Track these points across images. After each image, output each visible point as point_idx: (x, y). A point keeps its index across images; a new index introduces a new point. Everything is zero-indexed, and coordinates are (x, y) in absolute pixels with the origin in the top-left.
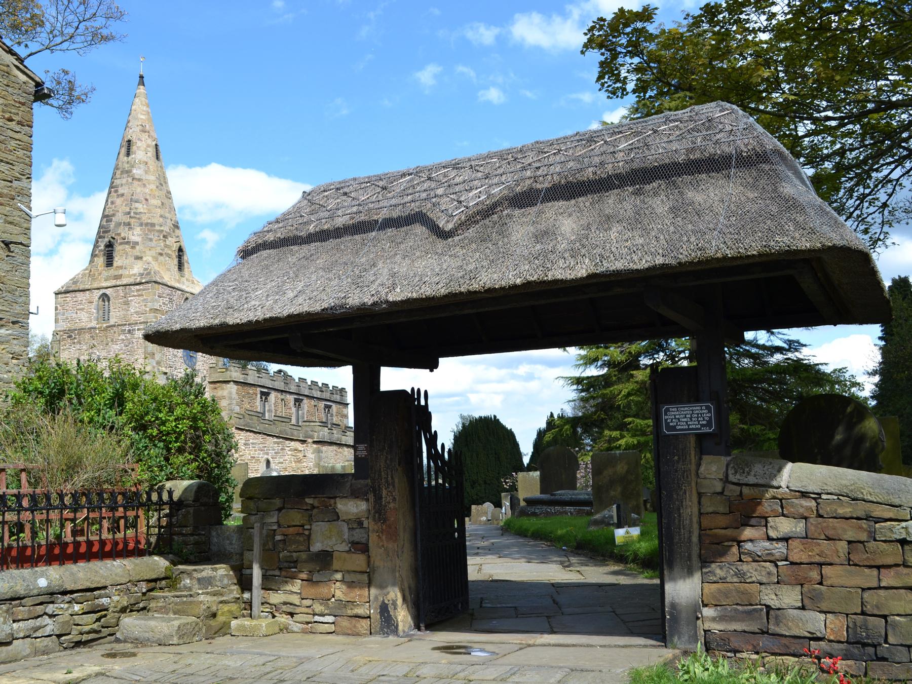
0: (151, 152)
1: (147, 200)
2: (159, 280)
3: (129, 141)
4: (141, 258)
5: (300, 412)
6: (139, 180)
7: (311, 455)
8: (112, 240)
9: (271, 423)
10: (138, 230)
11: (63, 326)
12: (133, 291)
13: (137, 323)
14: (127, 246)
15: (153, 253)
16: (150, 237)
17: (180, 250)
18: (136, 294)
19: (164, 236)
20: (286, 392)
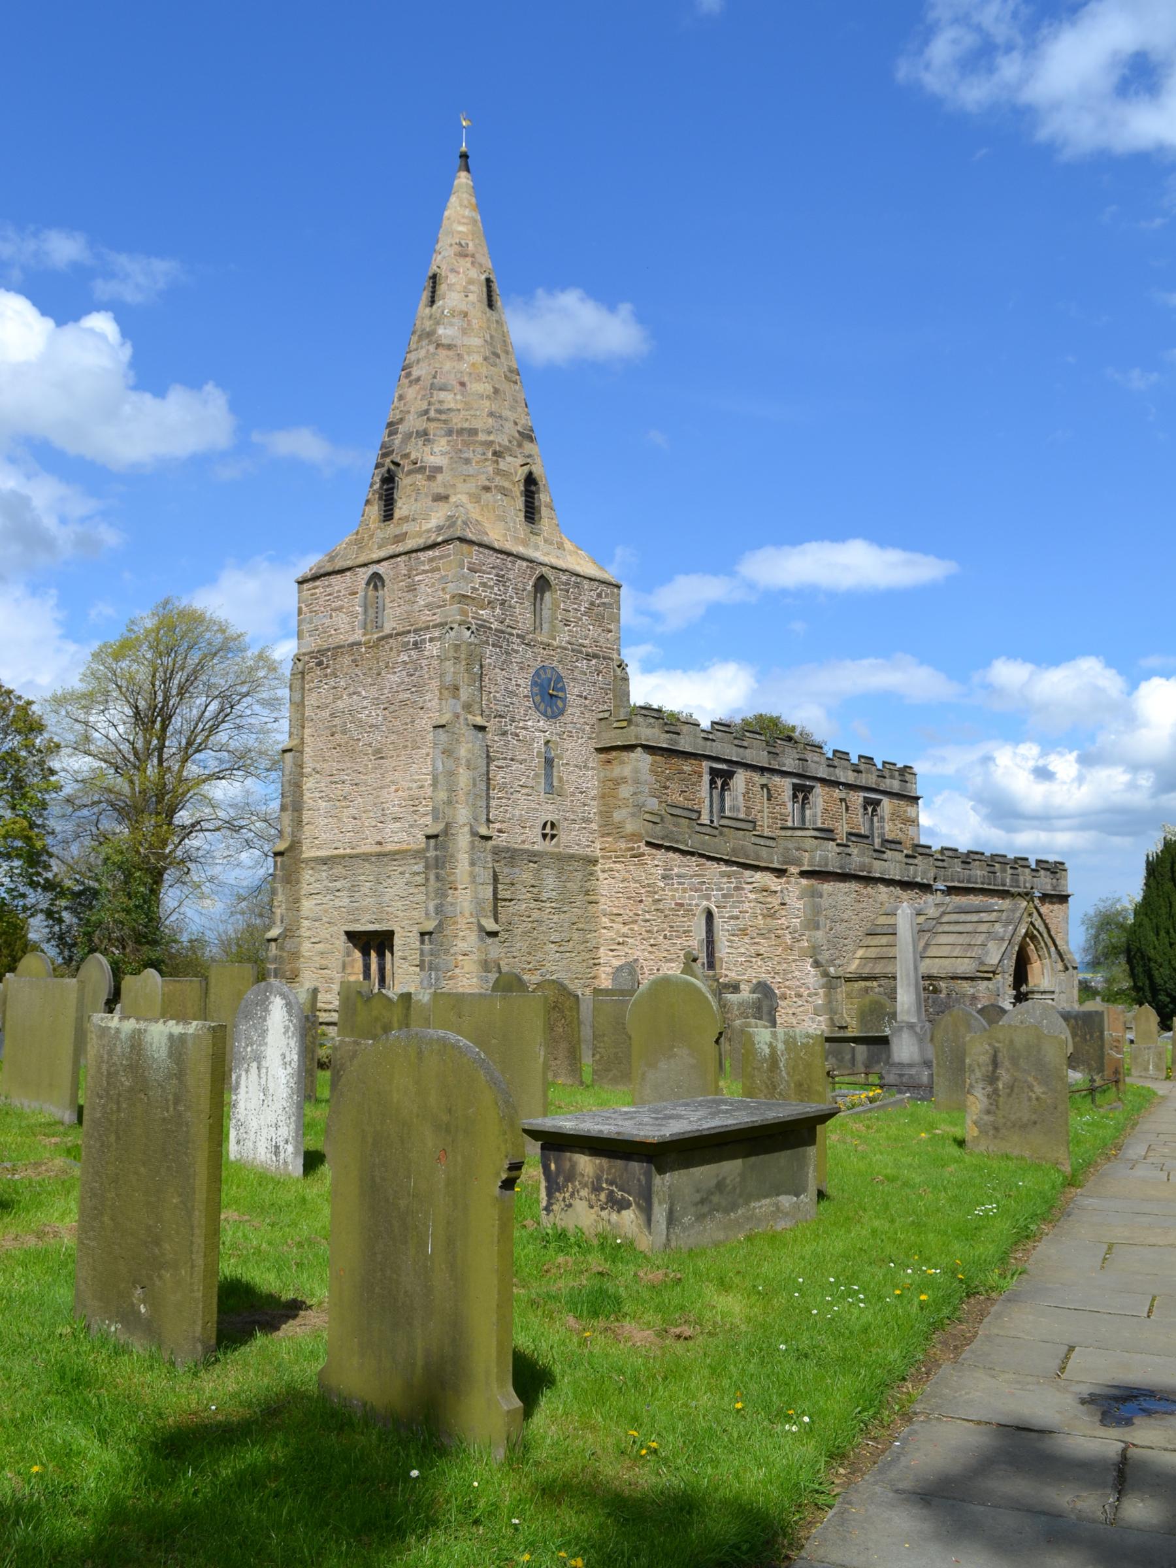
0: (477, 293)
1: (463, 384)
2: (470, 536)
3: (434, 277)
4: (446, 498)
5: (808, 812)
6: (449, 347)
7: (796, 903)
8: (392, 467)
9: (716, 832)
10: (442, 444)
11: (312, 643)
12: (423, 563)
13: (428, 628)
14: (419, 476)
15: (471, 486)
16: (465, 455)
17: (530, 481)
18: (427, 567)
19: (495, 453)
20: (772, 771)
